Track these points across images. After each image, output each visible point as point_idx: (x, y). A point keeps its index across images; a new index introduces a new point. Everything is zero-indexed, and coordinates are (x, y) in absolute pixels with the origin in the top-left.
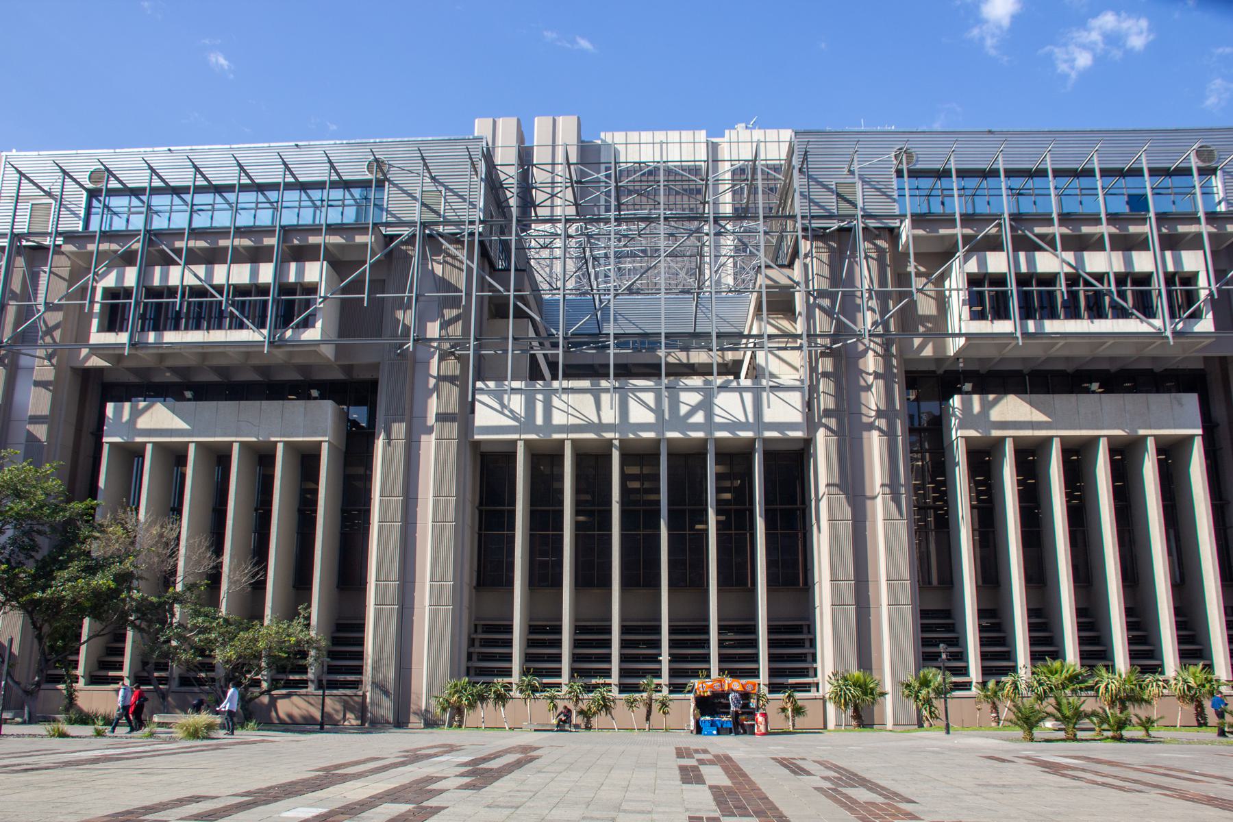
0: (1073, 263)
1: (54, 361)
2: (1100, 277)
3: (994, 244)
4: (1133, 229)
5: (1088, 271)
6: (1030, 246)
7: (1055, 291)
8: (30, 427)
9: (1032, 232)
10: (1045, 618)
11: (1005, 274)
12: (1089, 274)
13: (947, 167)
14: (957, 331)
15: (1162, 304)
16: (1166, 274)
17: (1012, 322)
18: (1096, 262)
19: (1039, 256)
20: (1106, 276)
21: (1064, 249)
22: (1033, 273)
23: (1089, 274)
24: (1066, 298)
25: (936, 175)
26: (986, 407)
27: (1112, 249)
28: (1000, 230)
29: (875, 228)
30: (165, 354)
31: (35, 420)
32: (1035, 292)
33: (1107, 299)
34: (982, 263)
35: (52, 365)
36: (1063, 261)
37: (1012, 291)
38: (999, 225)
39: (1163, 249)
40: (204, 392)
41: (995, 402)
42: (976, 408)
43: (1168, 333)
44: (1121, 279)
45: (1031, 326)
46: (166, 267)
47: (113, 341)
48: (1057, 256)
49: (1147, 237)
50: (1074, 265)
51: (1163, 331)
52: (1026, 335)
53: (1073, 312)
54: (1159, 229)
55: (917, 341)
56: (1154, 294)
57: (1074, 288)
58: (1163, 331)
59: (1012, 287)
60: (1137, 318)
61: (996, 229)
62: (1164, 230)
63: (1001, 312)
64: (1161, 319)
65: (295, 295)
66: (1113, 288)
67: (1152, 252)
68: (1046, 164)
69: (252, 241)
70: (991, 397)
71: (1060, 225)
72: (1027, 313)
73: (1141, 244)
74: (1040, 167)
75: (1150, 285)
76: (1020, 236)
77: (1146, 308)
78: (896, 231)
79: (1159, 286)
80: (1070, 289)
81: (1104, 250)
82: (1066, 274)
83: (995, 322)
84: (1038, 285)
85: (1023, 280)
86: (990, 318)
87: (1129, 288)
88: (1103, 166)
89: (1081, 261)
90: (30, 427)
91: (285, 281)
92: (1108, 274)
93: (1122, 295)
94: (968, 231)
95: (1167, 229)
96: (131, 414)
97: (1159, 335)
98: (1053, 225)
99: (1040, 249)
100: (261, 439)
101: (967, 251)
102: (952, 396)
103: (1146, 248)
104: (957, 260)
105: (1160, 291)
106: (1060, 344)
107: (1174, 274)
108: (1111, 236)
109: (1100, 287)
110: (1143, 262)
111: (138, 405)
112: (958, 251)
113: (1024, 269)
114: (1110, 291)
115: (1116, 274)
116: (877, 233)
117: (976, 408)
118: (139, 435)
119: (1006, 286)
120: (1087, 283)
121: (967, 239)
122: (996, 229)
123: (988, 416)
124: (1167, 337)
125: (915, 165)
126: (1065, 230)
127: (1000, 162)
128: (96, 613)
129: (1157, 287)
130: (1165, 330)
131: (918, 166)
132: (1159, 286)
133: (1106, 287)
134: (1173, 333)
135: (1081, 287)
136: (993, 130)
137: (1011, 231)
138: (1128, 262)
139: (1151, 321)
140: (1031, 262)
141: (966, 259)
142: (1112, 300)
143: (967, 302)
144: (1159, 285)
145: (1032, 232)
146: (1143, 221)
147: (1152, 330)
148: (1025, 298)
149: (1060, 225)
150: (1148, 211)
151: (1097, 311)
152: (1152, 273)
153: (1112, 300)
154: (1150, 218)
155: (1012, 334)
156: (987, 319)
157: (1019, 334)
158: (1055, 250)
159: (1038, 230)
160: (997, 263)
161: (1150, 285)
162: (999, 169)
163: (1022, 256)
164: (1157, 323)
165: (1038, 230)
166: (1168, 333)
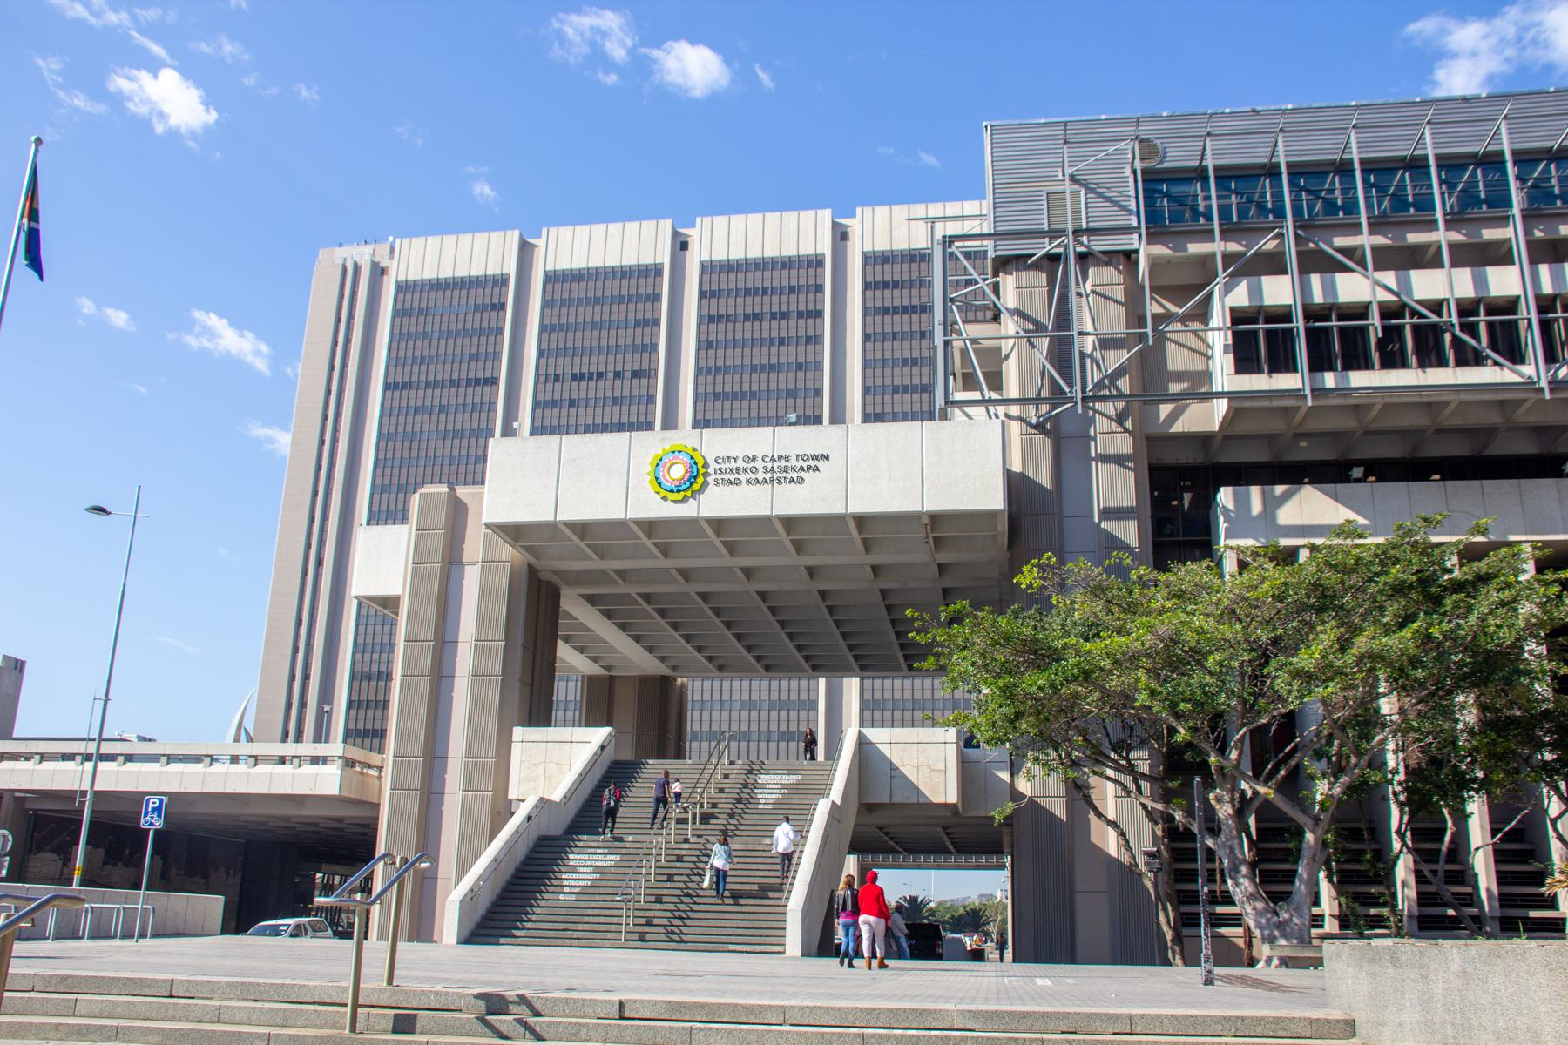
0: (1394, 287)
1: (1128, 424)
2: (1437, 306)
3: (1274, 263)
4: (1489, 234)
5: (1416, 297)
6: (1329, 265)
7: (1367, 326)
8: (1109, 526)
9: (1330, 245)
10: (1460, 863)
11: (1290, 306)
12: (1419, 302)
13: (1274, 160)
14: (1220, 390)
15: (1533, 342)
16: (1539, 298)
17: (1299, 375)
18: (1427, 285)
19: (1340, 278)
20: (1445, 304)
21: (1376, 269)
22: (1333, 304)
23: (1418, 302)
24: (1380, 335)
25: (1547, 156)
26: (1271, 505)
27: (1454, 265)
28: (1282, 243)
29: (1104, 252)
30: (1358, 406)
31: (1110, 513)
32: (1261, 334)
33: (1447, 337)
34: (1256, 291)
35: (1126, 430)
36: (1377, 283)
37: (1297, 327)
38: (1280, 236)
39: (1534, 261)
40: (1383, 470)
41: (1285, 497)
42: (1256, 507)
43: (1543, 384)
44: (1467, 309)
45: (1329, 380)
46: (1559, 265)
47: (1265, 387)
48: (1367, 277)
49: (1510, 249)
50: (1395, 288)
51: (1535, 380)
52: (1319, 392)
53: (1393, 360)
54: (1528, 232)
55: (1165, 410)
56: (1523, 325)
57: (1471, 319)
58: (1535, 380)
59: (1299, 323)
60: (1496, 363)
61: (1276, 242)
62: (1538, 234)
63: (1282, 362)
64: (1533, 366)
65: (1258, 323)
66: (1455, 319)
67: (1290, 276)
68: (1351, 153)
69: (1169, 248)
70: (1279, 489)
71: (1448, 228)
72: (1319, 363)
73: (1499, 255)
74: (1489, 148)
75: (1515, 313)
76: (1311, 252)
77: (1510, 348)
78: (1133, 256)
79: (1529, 313)
80: (1386, 322)
81: (1441, 266)
82: (1381, 305)
83: (1274, 375)
84: (1340, 318)
85: (1312, 313)
86: (1266, 371)
87: (1482, 318)
88: (1517, 146)
89: (1405, 285)
90: (1109, 526)
91: (1309, 302)
92: (1447, 300)
93: (1471, 329)
94: (1233, 247)
95: (1541, 231)
96: (1264, 504)
97: (1530, 386)
98: (1437, 229)
99: (1345, 269)
100: (1492, 537)
101: (1231, 275)
102: (1216, 491)
103: (1282, 270)
104: (1217, 287)
105: (1529, 320)
106: (1530, 403)
107: (1553, 298)
108: (1452, 246)
109: (1434, 319)
110: (1504, 281)
111: (1273, 491)
112: (1217, 276)
113: (1318, 297)
114: (1452, 325)
115: (1459, 302)
116: (1106, 259)
117: (1256, 507)
118: (1287, 536)
119: (1291, 322)
120: (1414, 313)
121: (1228, 259)
122: (1276, 242)
123: (1274, 518)
124: (1541, 390)
125: (1161, 162)
126: (1456, 237)
127: (1354, 150)
128: (1158, 851)
129: (1525, 315)
130: (1539, 378)
131: (1165, 165)
132: (1529, 313)
133: (1445, 318)
134: (1550, 383)
135: (1482, 317)
136: (1259, 108)
137: (1297, 244)
138: (1480, 282)
139: (1518, 367)
140: (1329, 288)
141: (1228, 289)
142: (1455, 339)
143: (1231, 349)
144: (1528, 312)
145: (1330, 245)
146: (1504, 221)
147: (1518, 379)
148: (1317, 339)
149: (1448, 228)
150: (1510, 206)
151: (1430, 354)
152: (1518, 298)
153: (1455, 339)
154: (1513, 216)
155: (1299, 390)
156: (1263, 373)
157: (1308, 392)
158: (1365, 268)
159: (1339, 241)
160: (1278, 291)
161: (1516, 313)
162: (1352, 159)
163: (1315, 280)
164: (1528, 370)
165: (1339, 241)
166: (1543, 384)
